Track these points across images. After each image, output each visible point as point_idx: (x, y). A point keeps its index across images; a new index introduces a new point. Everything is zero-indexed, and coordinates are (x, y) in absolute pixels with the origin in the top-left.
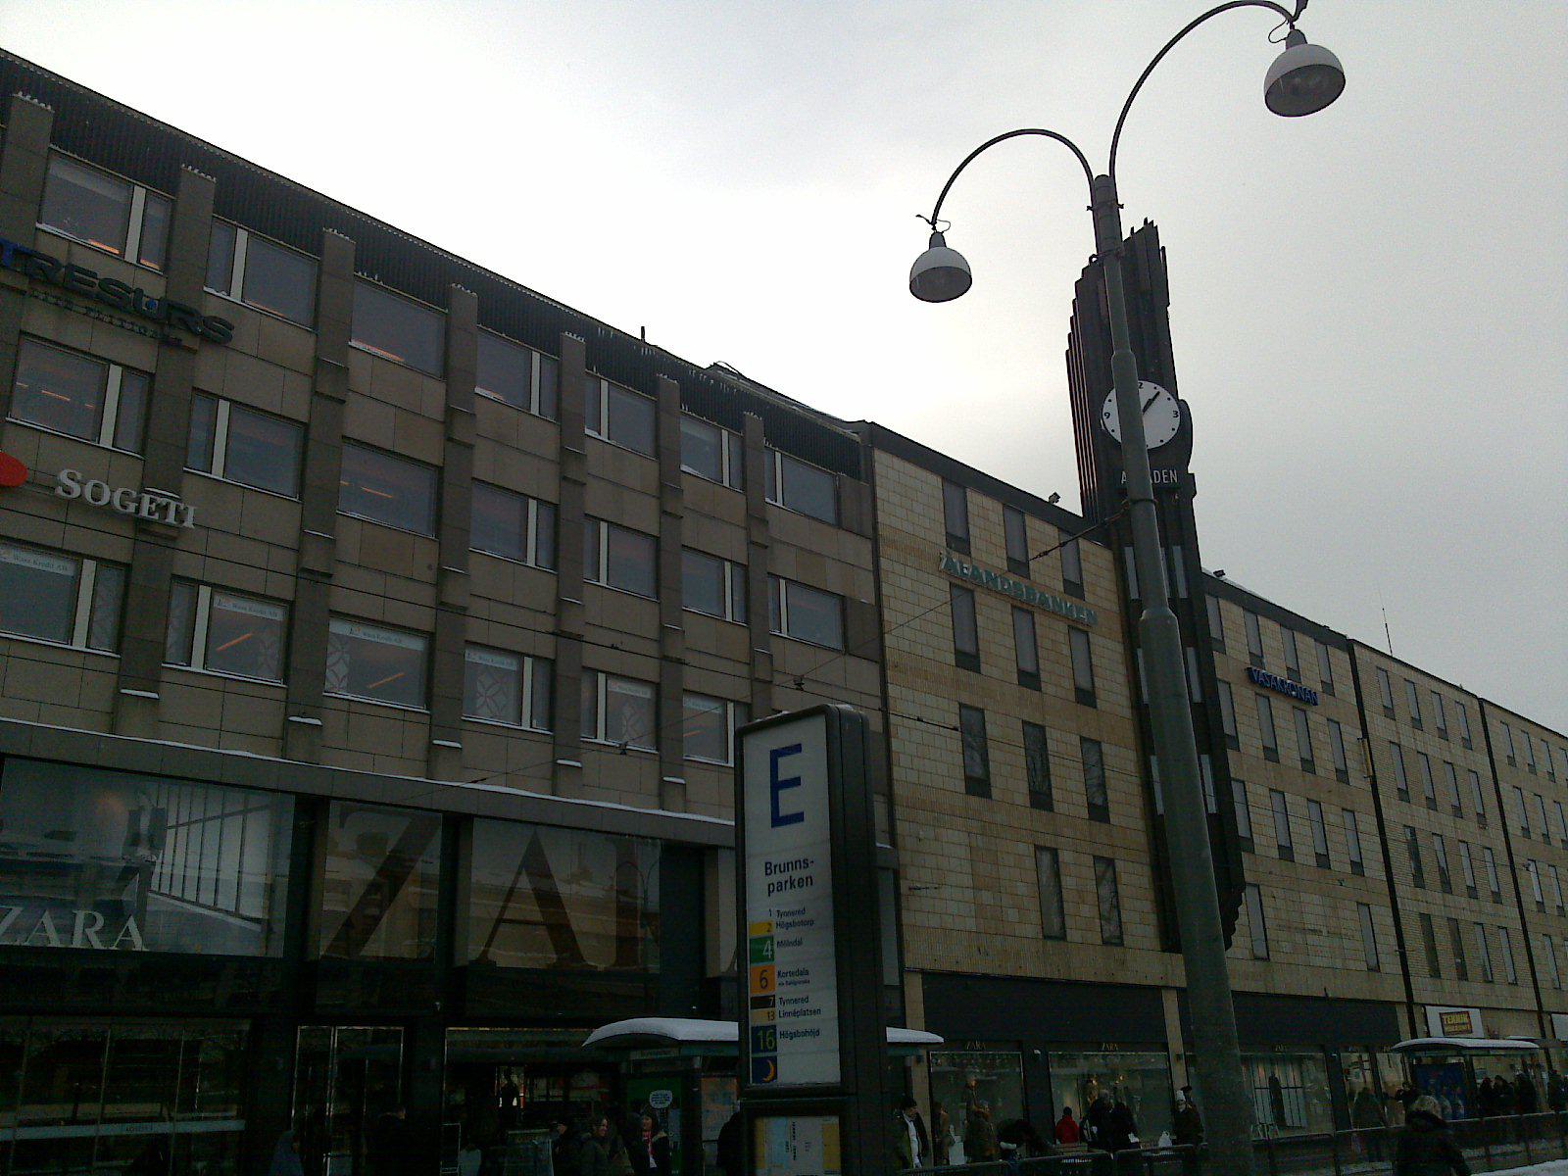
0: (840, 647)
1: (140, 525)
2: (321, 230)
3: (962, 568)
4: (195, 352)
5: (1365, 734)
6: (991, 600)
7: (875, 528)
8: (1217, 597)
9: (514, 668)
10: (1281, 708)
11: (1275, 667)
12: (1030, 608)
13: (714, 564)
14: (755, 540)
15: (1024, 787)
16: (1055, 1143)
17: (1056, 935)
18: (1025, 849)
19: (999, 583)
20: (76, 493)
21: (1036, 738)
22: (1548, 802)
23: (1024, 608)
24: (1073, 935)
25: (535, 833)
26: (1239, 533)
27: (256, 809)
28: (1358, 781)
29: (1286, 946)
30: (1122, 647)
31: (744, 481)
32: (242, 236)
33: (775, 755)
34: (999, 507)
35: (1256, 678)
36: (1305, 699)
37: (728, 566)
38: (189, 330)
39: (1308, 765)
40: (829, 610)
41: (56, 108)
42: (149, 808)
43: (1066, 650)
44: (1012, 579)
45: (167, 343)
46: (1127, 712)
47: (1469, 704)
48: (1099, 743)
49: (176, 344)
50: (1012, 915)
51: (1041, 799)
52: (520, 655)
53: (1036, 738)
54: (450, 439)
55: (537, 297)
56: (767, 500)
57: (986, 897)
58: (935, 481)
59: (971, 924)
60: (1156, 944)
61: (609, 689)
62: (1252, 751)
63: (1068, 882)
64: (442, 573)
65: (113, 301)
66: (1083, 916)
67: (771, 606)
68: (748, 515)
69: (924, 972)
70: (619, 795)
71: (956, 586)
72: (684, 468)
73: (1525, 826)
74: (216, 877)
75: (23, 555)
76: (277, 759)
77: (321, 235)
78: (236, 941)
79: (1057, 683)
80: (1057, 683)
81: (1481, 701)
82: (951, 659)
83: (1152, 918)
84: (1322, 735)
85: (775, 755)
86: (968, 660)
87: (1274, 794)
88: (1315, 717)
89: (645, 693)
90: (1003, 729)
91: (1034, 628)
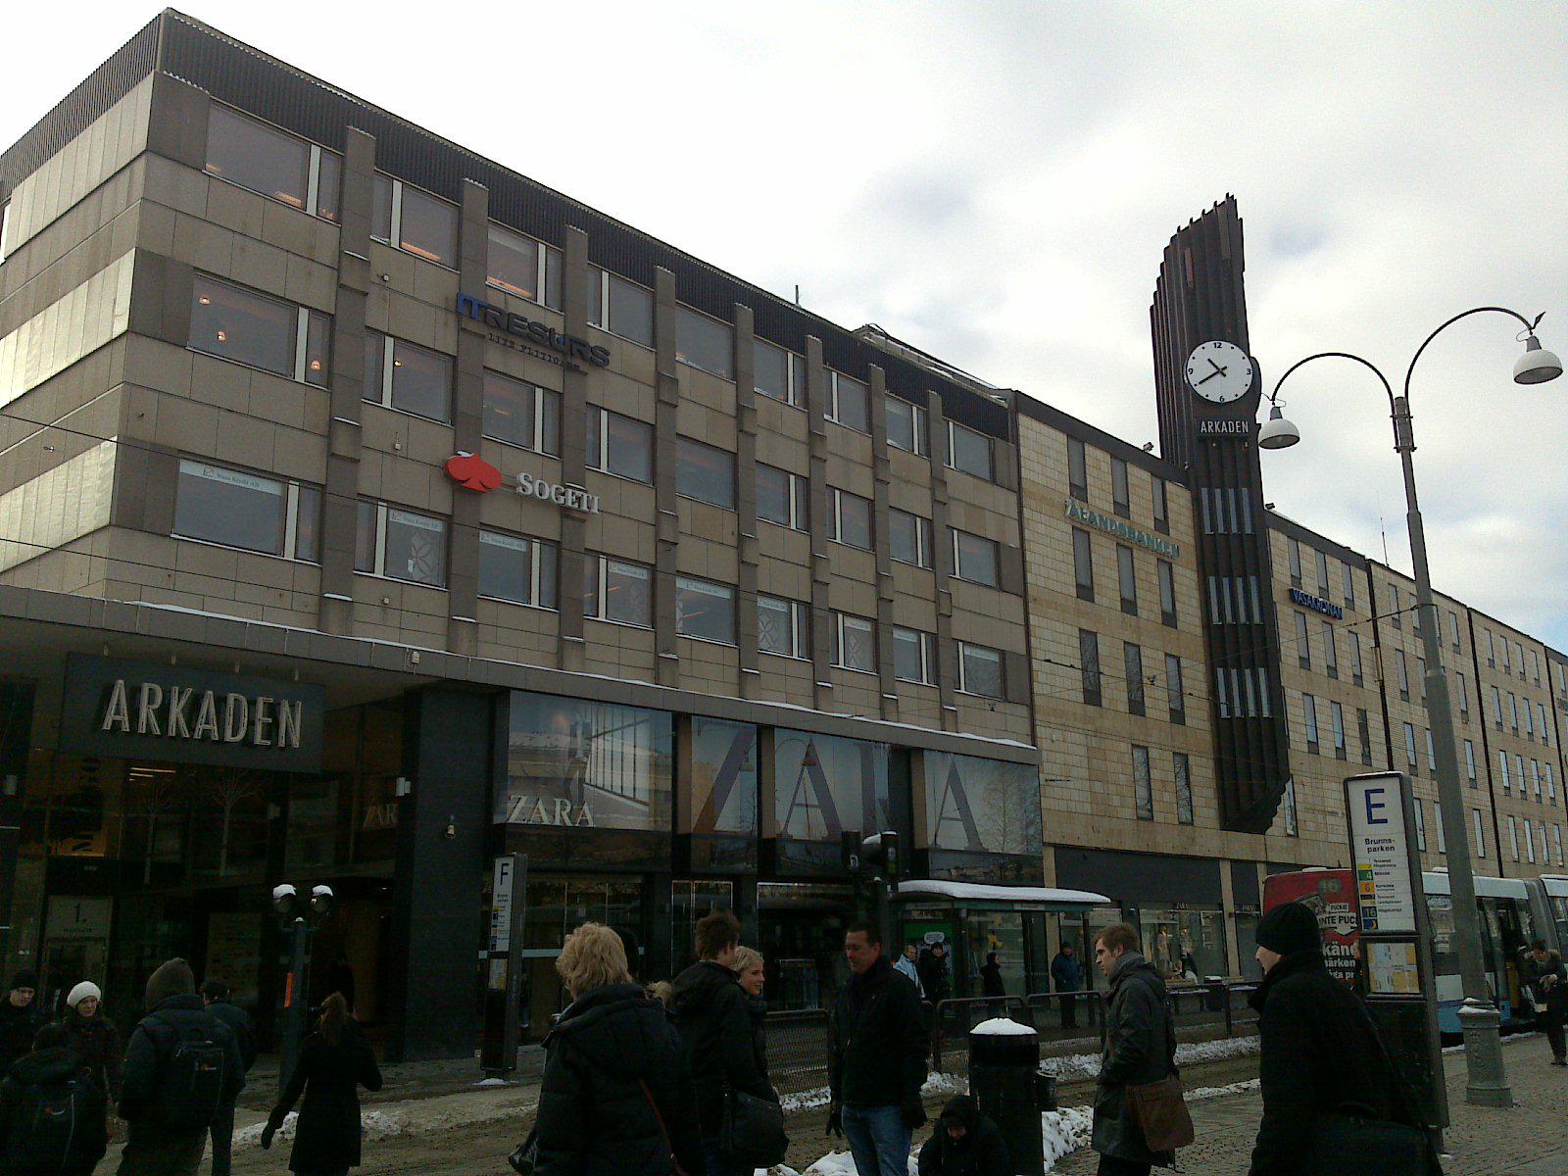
0: (994, 584)
1: (564, 512)
2: (652, 268)
3: (1083, 513)
4: (586, 374)
5: (1377, 644)
6: (1103, 540)
7: (1019, 484)
8: (1125, 462)
9: (524, 549)
10: (1314, 620)
11: (1310, 588)
12: (1130, 545)
13: (908, 518)
14: (349, 283)
15: (1124, 696)
16: (114, 1102)
17: (1146, 816)
18: (1125, 747)
19: (1109, 525)
20: (530, 492)
21: (1132, 649)
22: (1518, 698)
23: (1126, 545)
24: (1158, 817)
25: (811, 740)
26: (1321, 485)
27: (642, 722)
28: (1370, 685)
29: (1311, 826)
30: (1196, 576)
31: (339, 211)
32: (397, 186)
33: (503, 865)
34: (1108, 458)
35: (1295, 597)
36: (1333, 614)
37: (792, 477)
38: (584, 359)
39: (1333, 671)
40: (985, 552)
41: (754, 311)
42: (581, 723)
43: (1155, 580)
44: (1118, 520)
45: (569, 368)
46: (1199, 631)
47: (1460, 613)
48: (1095, 634)
49: (574, 369)
50: (1116, 801)
51: (1137, 707)
52: (529, 538)
53: (1132, 649)
54: (741, 431)
55: (349, 98)
56: (826, 417)
57: (1098, 786)
58: (1062, 438)
59: (1087, 808)
60: (1216, 824)
61: (610, 571)
62: (1290, 661)
63: (1155, 774)
64: (741, 538)
65: (536, 338)
66: (1165, 800)
67: (590, 437)
68: (933, 478)
69: (1055, 846)
70: (852, 705)
71: (1077, 528)
72: (889, 442)
73: (1499, 720)
74: (622, 775)
75: (509, 540)
76: (1025, 746)
77: (654, 271)
78: (636, 818)
79: (1150, 607)
80: (1150, 607)
81: (1470, 610)
82: (1073, 591)
83: (1214, 803)
84: (1345, 646)
85: (503, 865)
86: (1085, 592)
87: (1128, 648)
88: (1340, 630)
89: (437, 526)
90: (1110, 652)
91: (1132, 561)
